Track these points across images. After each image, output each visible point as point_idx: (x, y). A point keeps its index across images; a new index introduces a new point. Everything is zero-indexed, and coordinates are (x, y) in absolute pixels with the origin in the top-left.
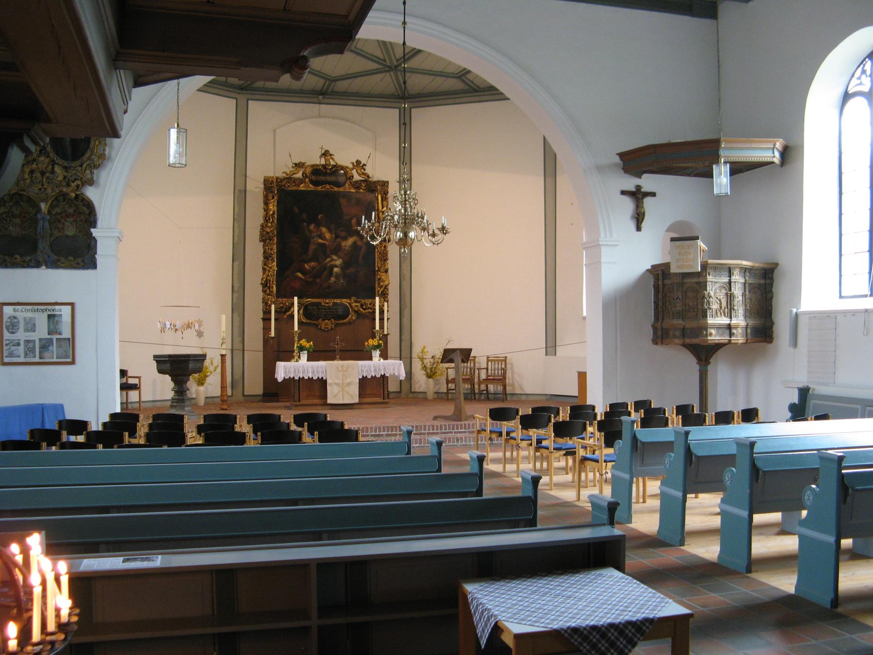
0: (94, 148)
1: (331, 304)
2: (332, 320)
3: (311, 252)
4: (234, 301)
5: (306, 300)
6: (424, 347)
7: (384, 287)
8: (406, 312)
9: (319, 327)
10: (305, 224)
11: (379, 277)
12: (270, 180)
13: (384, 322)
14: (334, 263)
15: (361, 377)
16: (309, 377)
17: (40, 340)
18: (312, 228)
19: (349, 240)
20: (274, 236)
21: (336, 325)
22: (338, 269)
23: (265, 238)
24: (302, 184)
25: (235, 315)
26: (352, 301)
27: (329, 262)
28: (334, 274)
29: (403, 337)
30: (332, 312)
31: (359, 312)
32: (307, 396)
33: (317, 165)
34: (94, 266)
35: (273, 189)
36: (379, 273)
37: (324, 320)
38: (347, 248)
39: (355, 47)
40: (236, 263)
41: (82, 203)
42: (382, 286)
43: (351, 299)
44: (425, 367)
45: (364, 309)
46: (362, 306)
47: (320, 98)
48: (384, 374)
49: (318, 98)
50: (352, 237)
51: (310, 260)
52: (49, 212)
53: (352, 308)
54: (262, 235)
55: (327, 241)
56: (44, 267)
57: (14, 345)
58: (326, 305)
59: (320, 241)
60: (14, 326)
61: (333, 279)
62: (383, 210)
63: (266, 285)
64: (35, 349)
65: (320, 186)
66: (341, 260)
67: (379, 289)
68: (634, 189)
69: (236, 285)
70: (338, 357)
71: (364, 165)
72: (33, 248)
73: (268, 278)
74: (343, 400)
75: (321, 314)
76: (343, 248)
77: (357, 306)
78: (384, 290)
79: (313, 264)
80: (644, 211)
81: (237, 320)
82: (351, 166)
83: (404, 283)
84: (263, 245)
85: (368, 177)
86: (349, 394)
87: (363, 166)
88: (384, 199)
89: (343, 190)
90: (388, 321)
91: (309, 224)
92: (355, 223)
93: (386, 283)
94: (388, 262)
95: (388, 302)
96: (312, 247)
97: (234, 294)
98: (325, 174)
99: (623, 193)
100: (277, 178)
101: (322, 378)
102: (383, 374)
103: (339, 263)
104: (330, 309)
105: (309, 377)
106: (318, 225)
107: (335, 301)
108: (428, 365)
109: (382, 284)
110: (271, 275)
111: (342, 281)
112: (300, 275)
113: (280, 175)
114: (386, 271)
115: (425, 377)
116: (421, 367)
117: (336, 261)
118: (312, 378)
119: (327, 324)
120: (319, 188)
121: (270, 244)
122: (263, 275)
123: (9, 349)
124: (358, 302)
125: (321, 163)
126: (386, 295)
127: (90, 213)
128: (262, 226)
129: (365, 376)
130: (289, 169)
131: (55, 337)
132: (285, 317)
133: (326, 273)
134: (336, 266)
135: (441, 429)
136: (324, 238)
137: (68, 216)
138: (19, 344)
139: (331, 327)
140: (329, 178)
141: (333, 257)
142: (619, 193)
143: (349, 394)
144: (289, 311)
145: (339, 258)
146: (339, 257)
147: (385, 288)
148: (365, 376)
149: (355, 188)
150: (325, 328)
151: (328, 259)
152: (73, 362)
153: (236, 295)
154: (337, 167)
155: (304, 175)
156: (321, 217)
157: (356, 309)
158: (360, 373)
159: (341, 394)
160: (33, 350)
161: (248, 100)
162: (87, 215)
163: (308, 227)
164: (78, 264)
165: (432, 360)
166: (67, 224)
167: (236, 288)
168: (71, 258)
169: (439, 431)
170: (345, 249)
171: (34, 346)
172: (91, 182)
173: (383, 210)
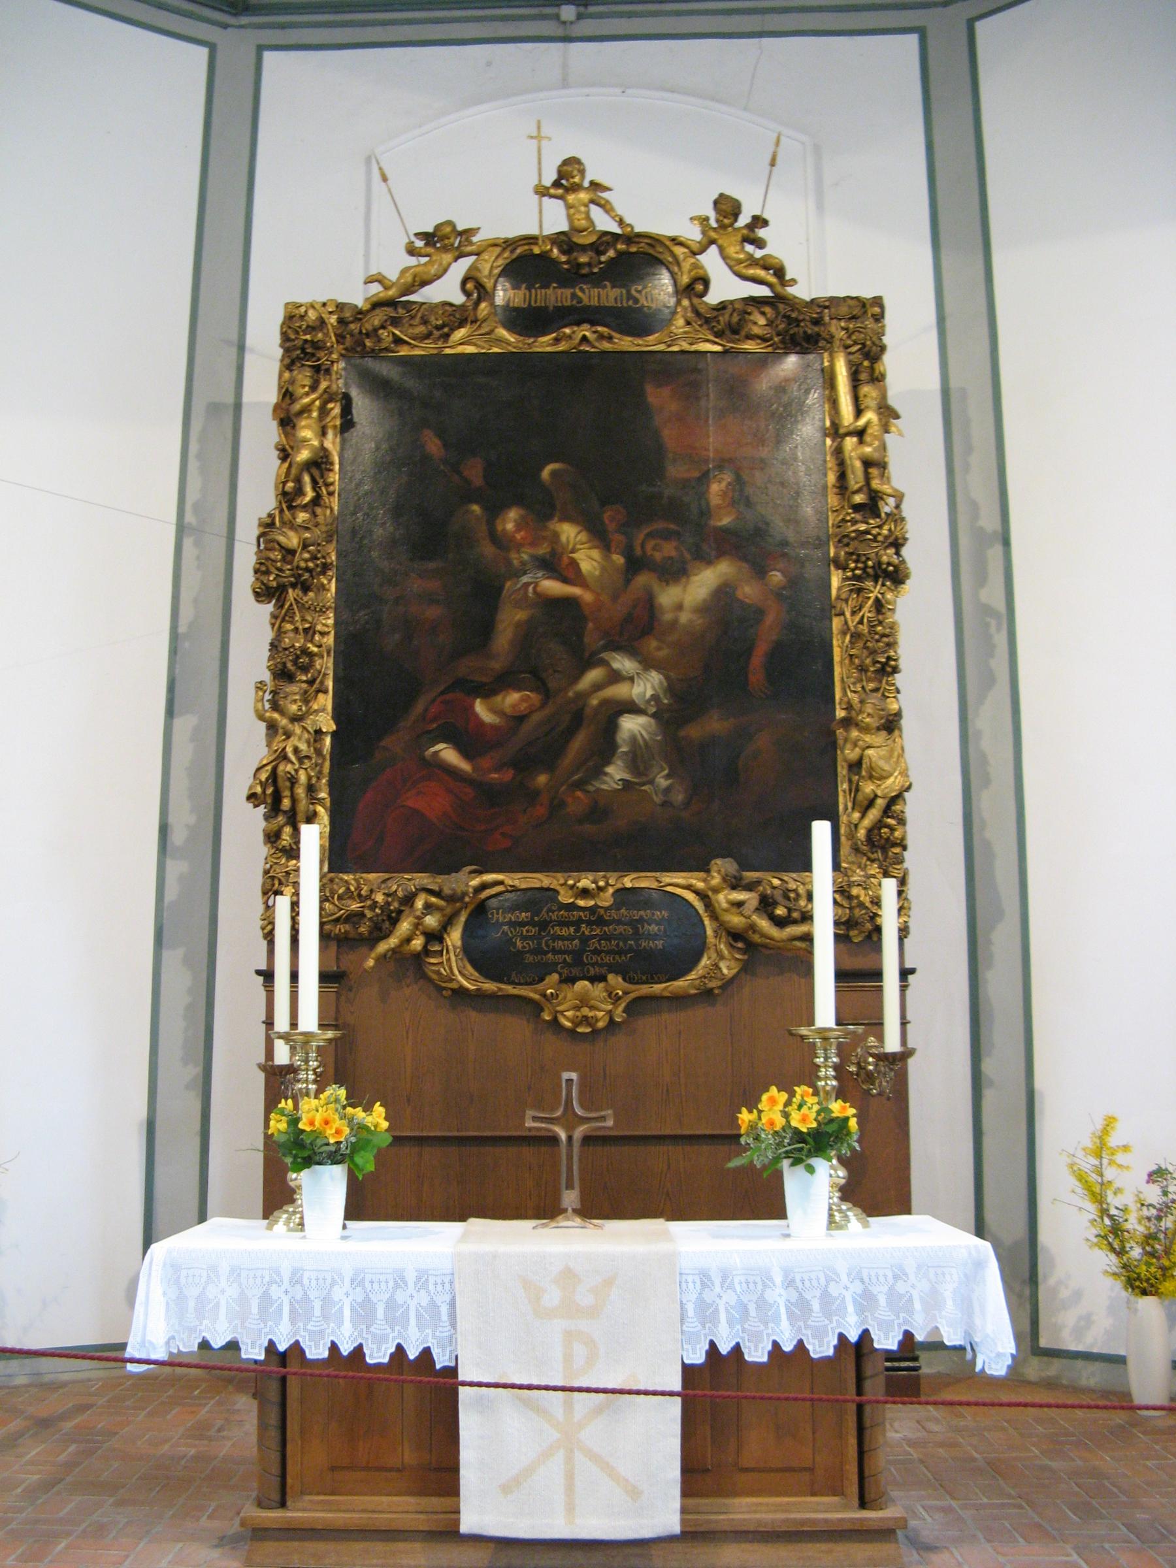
1: (606, 899)
2: (610, 977)
3: (504, 637)
4: (170, 895)
5: (475, 882)
6: (1109, 1123)
7: (880, 803)
8: (1002, 939)
9: (547, 1017)
10: (476, 508)
11: (851, 754)
12: (312, 315)
13: (880, 989)
14: (620, 691)
15: (697, 1357)
16: (334, 1347)
18: (510, 526)
19: (695, 579)
20: (325, 567)
21: (637, 1007)
24: (461, 325)
25: (172, 957)
26: (716, 880)
27: (597, 687)
29: (988, 1066)
30: (607, 937)
31: (756, 938)
32: (333, 1469)
33: (531, 240)
35: (321, 354)
36: (855, 733)
37: (571, 980)
40: (184, 725)
42: (871, 803)
43: (708, 871)
44: (1116, 1229)
45: (780, 923)
46: (766, 905)
48: (865, 1335)
49: (557, 17)
50: (709, 563)
51: (503, 682)
53: (714, 916)
58: (581, 903)
59: (552, 587)
61: (616, 772)
62: (861, 422)
65: (544, 334)
67: (856, 815)
69: (183, 819)
70: (570, 1198)
73: (281, 768)
74: (570, 1508)
75: (555, 952)
76: (668, 617)
77: (739, 904)
78: (879, 825)
79: (512, 699)
81: (179, 981)
82: (693, 234)
83: (985, 802)
84: (274, 616)
86: (608, 1469)
89: (661, 347)
90: (903, 988)
91: (494, 510)
92: (724, 494)
93: (892, 784)
94: (898, 679)
95: (902, 882)
97: (170, 864)
98: (574, 276)
100: (340, 307)
101: (426, 1353)
102: (853, 1337)
103: (649, 693)
104: (601, 922)
105: (334, 1347)
107: (628, 882)
108: (1134, 1225)
109: (868, 788)
110: (296, 750)
111: (663, 782)
113: (357, 296)
114: (891, 724)
115: (1116, 1289)
116: (1091, 1233)
117: (631, 679)
118: (358, 1351)
119: (584, 1001)
120: (544, 344)
121: (303, 607)
124: (750, 887)
126: (897, 850)
129: (724, 1348)
132: (371, 963)
133: (578, 742)
134: (632, 708)
139: (610, 1013)
140: (590, 296)
141: (616, 665)
143: (608, 1469)
144: (387, 936)
146: (648, 664)
147: (887, 811)
148: (724, 1348)
149: (719, 334)
150: (577, 1022)
151: (594, 675)
153: (175, 868)
156: (554, 474)
157: (735, 920)
158: (692, 1324)
159: (555, 1468)
161: (261, 49)
165: (1153, 1194)
167: (178, 837)
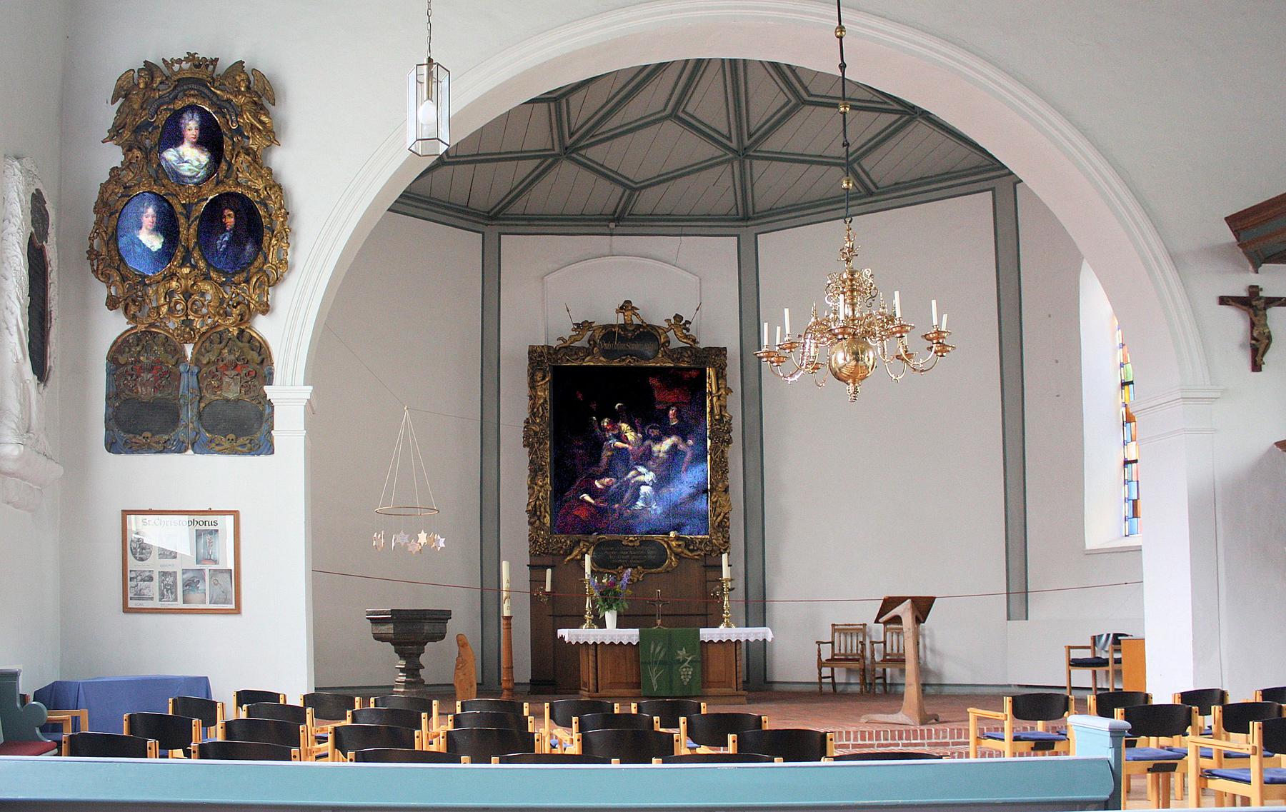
0: (269, 250)
12: (539, 350)
14: (641, 478)
17: (185, 571)
18: (605, 424)
22: (648, 487)
23: (530, 440)
27: (634, 477)
28: (642, 496)
33: (613, 326)
34: (270, 450)
38: (661, 455)
39: (683, 111)
41: (248, 345)
45: (691, 551)
47: (611, 226)
49: (608, 226)
52: (197, 361)
54: (527, 437)
55: (629, 444)
56: (190, 452)
57: (143, 580)
59: (619, 444)
60: (143, 549)
61: (640, 504)
63: (535, 514)
64: (176, 586)
66: (652, 474)
68: (1244, 294)
71: (687, 322)
72: (171, 416)
73: (537, 503)
76: (655, 455)
77: (679, 545)
78: (721, 521)
80: (1269, 332)
82: (666, 325)
84: (529, 452)
85: (694, 341)
87: (685, 324)
88: (720, 375)
91: (600, 420)
96: (606, 454)
99: (1223, 301)
106: (615, 419)
109: (718, 510)
112: (587, 498)
113: (555, 344)
120: (616, 363)
122: (529, 499)
123: (137, 585)
125: (619, 323)
127: (262, 361)
128: (527, 422)
130: (567, 332)
131: (207, 567)
134: (644, 484)
135: (878, 738)
136: (625, 440)
137: (226, 367)
138: (151, 579)
141: (639, 470)
142: (1216, 301)
145: (649, 471)
147: (724, 517)
151: (632, 473)
152: (237, 610)
154: (644, 328)
155: (592, 342)
160: (172, 588)
161: (500, 234)
162: (258, 364)
163: (599, 424)
164: (243, 446)
166: (226, 379)
168: (232, 436)
169: (874, 742)
170: (658, 457)
171: (175, 582)
172: (266, 309)
173: (720, 393)
